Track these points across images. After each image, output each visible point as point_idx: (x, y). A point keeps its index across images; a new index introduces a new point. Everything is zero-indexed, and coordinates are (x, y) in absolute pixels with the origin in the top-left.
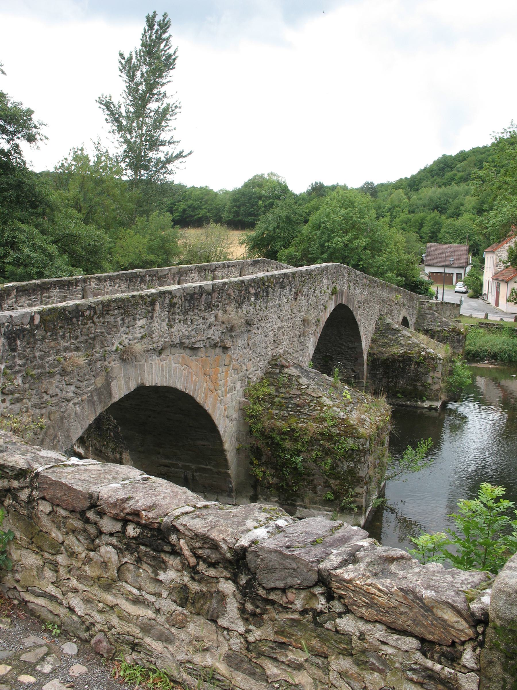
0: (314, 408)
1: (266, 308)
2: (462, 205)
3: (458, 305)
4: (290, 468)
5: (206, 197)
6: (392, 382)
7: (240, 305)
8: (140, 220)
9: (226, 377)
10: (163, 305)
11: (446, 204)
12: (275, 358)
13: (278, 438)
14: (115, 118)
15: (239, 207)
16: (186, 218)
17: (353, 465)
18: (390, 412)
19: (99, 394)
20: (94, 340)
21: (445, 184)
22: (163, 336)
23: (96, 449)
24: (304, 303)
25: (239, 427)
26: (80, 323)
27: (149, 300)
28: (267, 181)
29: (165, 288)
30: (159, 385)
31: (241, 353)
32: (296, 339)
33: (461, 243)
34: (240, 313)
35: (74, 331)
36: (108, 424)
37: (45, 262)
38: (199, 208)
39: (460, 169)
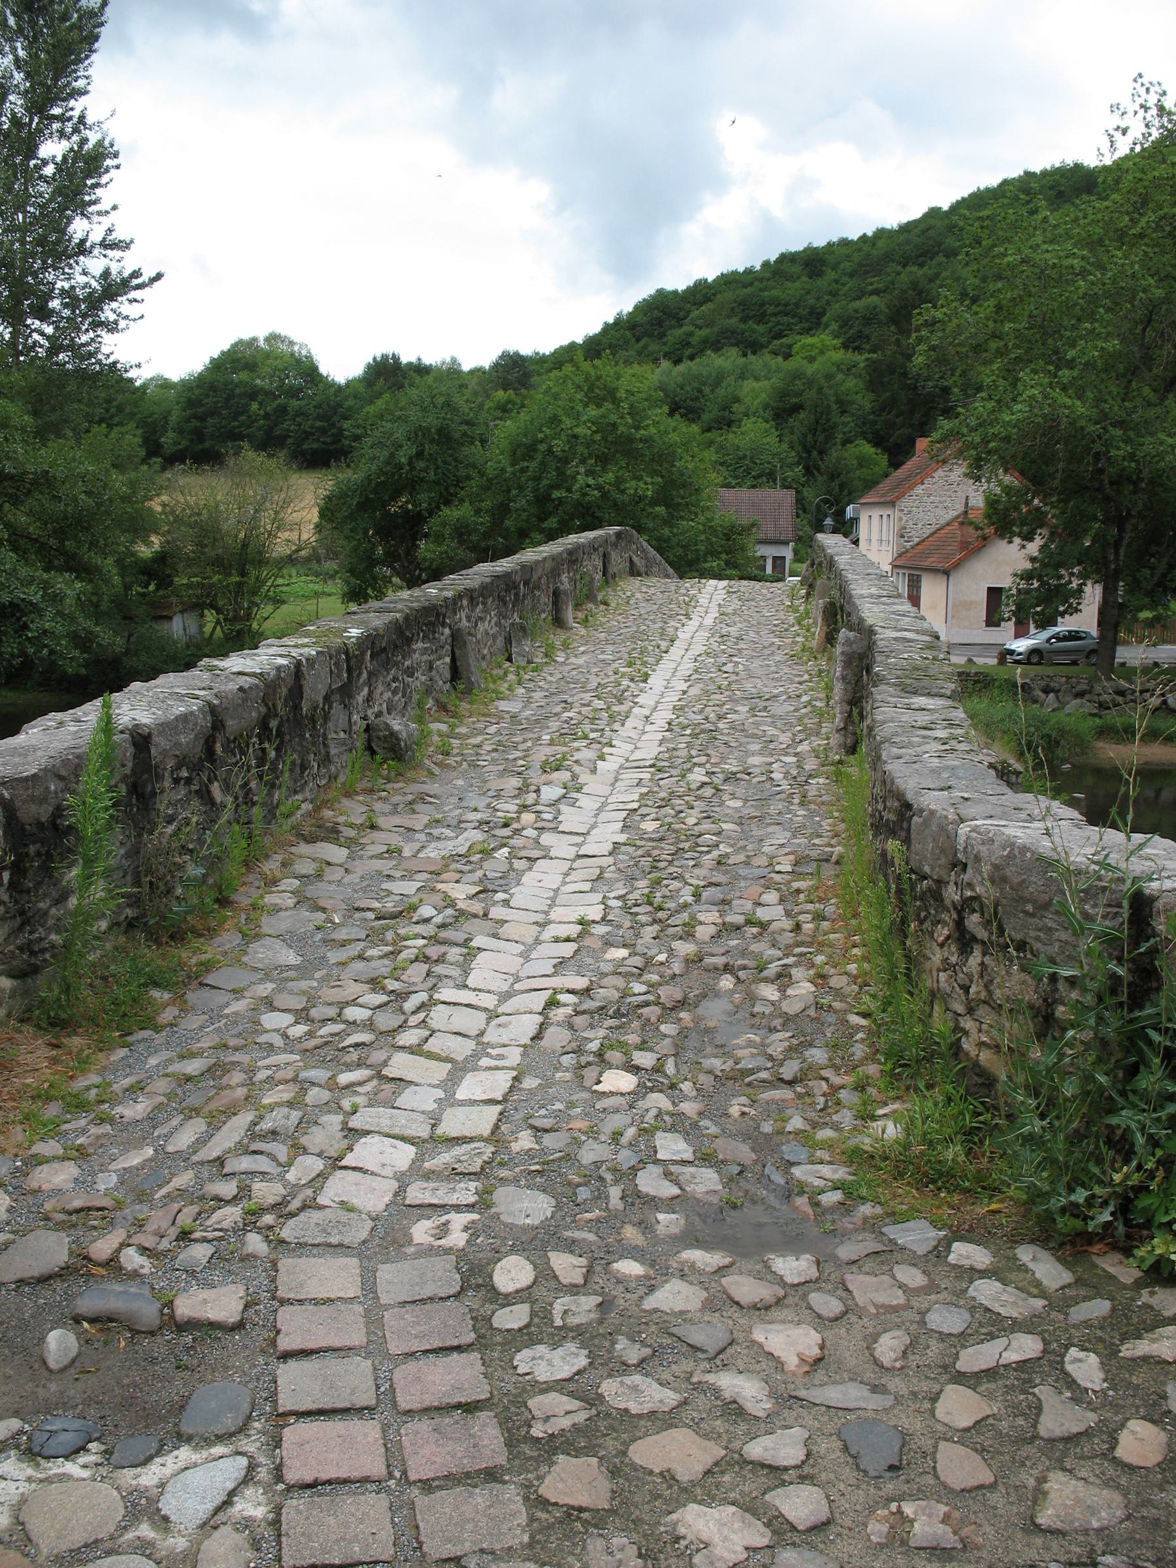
2: (737, 400)
11: (697, 399)
28: (268, 355)
33: (754, 487)
39: (699, 322)
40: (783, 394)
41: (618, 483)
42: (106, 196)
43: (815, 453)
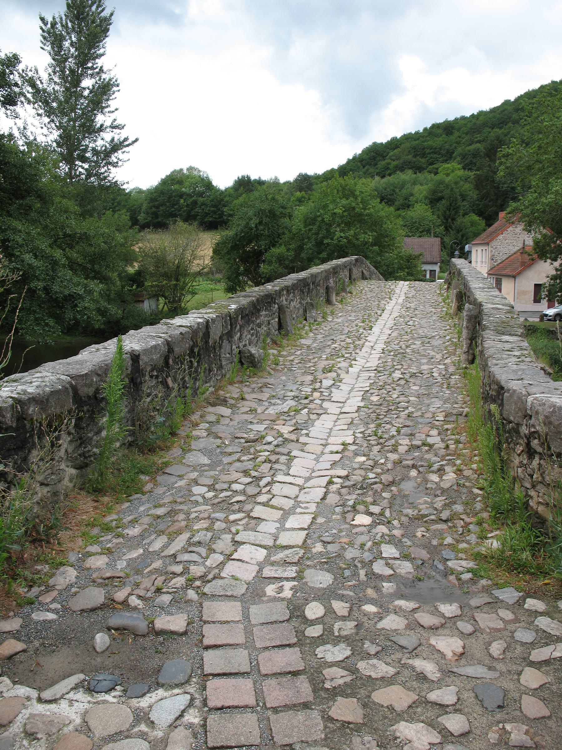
2: (412, 195)
11: (393, 194)
28: (188, 177)
33: (420, 237)
39: (393, 158)
40: (434, 192)
41: (355, 236)
42: (113, 104)
43: (450, 220)
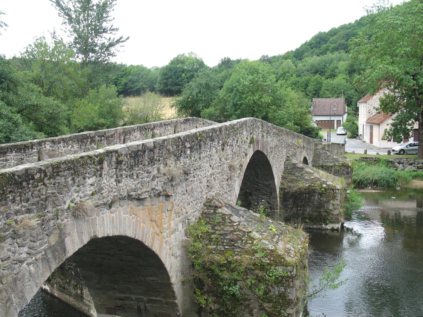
0: (246, 242)
1: (200, 159)
2: (337, 68)
3: (343, 145)
4: (229, 295)
5: (142, 73)
6: (300, 210)
7: (178, 158)
8: (92, 92)
9: (169, 221)
10: (110, 163)
11: (324, 68)
12: (209, 201)
13: (217, 271)
14: (65, 13)
15: (167, 79)
16: (128, 89)
17: (283, 290)
18: (307, 240)
19: (53, 252)
20: (46, 201)
21: (322, 54)
22: (112, 191)
23: (60, 286)
24: (229, 152)
25: (182, 262)
26: (30, 186)
27: (97, 159)
28: (188, 59)
29: (111, 148)
30: (111, 235)
31: (181, 199)
32: (225, 183)
33: (338, 97)
34: (178, 165)
35: (25, 194)
36: (70, 264)
37: (12, 128)
38: (137, 81)
39: (332, 42)
40: (352, 66)
42: (112, 14)
